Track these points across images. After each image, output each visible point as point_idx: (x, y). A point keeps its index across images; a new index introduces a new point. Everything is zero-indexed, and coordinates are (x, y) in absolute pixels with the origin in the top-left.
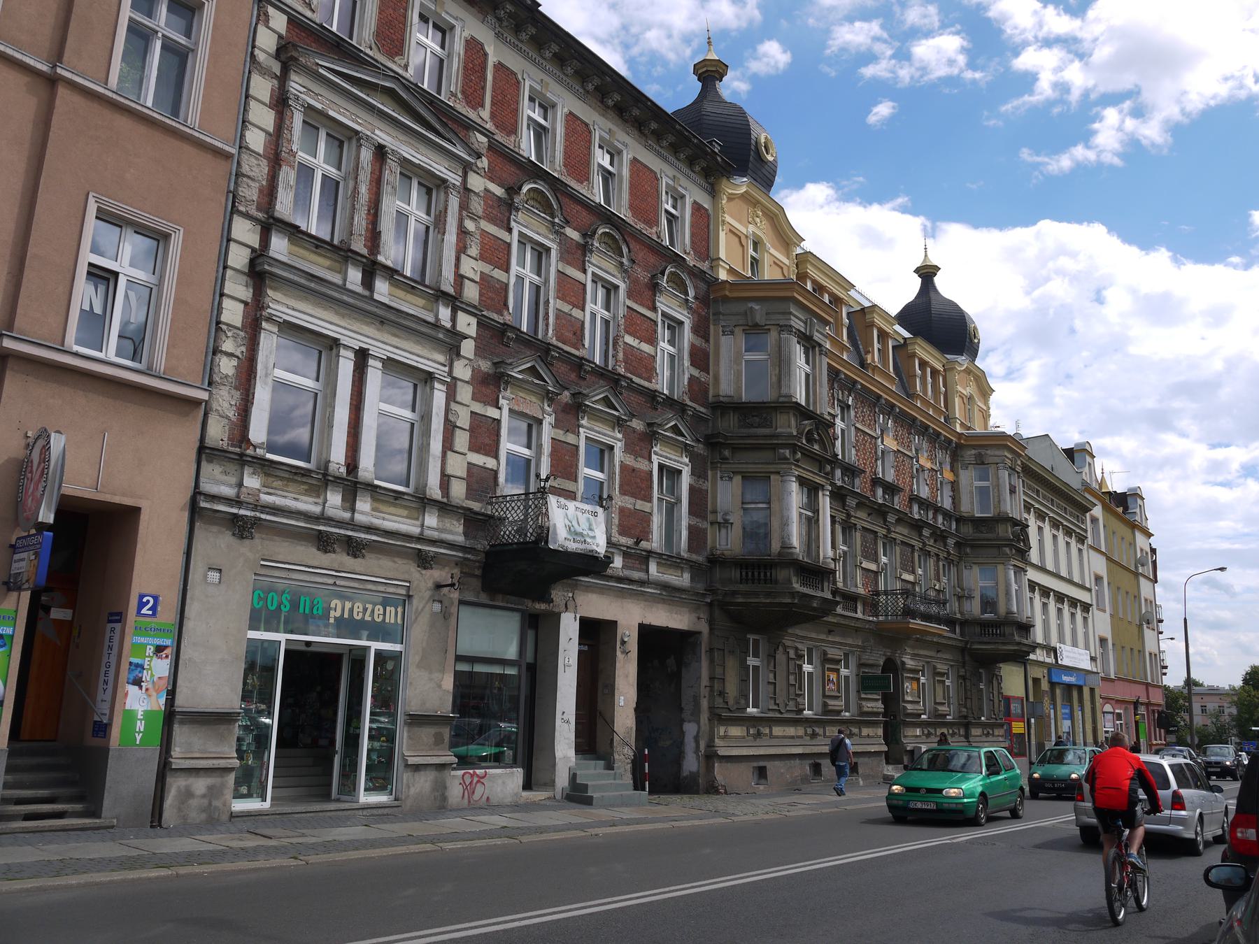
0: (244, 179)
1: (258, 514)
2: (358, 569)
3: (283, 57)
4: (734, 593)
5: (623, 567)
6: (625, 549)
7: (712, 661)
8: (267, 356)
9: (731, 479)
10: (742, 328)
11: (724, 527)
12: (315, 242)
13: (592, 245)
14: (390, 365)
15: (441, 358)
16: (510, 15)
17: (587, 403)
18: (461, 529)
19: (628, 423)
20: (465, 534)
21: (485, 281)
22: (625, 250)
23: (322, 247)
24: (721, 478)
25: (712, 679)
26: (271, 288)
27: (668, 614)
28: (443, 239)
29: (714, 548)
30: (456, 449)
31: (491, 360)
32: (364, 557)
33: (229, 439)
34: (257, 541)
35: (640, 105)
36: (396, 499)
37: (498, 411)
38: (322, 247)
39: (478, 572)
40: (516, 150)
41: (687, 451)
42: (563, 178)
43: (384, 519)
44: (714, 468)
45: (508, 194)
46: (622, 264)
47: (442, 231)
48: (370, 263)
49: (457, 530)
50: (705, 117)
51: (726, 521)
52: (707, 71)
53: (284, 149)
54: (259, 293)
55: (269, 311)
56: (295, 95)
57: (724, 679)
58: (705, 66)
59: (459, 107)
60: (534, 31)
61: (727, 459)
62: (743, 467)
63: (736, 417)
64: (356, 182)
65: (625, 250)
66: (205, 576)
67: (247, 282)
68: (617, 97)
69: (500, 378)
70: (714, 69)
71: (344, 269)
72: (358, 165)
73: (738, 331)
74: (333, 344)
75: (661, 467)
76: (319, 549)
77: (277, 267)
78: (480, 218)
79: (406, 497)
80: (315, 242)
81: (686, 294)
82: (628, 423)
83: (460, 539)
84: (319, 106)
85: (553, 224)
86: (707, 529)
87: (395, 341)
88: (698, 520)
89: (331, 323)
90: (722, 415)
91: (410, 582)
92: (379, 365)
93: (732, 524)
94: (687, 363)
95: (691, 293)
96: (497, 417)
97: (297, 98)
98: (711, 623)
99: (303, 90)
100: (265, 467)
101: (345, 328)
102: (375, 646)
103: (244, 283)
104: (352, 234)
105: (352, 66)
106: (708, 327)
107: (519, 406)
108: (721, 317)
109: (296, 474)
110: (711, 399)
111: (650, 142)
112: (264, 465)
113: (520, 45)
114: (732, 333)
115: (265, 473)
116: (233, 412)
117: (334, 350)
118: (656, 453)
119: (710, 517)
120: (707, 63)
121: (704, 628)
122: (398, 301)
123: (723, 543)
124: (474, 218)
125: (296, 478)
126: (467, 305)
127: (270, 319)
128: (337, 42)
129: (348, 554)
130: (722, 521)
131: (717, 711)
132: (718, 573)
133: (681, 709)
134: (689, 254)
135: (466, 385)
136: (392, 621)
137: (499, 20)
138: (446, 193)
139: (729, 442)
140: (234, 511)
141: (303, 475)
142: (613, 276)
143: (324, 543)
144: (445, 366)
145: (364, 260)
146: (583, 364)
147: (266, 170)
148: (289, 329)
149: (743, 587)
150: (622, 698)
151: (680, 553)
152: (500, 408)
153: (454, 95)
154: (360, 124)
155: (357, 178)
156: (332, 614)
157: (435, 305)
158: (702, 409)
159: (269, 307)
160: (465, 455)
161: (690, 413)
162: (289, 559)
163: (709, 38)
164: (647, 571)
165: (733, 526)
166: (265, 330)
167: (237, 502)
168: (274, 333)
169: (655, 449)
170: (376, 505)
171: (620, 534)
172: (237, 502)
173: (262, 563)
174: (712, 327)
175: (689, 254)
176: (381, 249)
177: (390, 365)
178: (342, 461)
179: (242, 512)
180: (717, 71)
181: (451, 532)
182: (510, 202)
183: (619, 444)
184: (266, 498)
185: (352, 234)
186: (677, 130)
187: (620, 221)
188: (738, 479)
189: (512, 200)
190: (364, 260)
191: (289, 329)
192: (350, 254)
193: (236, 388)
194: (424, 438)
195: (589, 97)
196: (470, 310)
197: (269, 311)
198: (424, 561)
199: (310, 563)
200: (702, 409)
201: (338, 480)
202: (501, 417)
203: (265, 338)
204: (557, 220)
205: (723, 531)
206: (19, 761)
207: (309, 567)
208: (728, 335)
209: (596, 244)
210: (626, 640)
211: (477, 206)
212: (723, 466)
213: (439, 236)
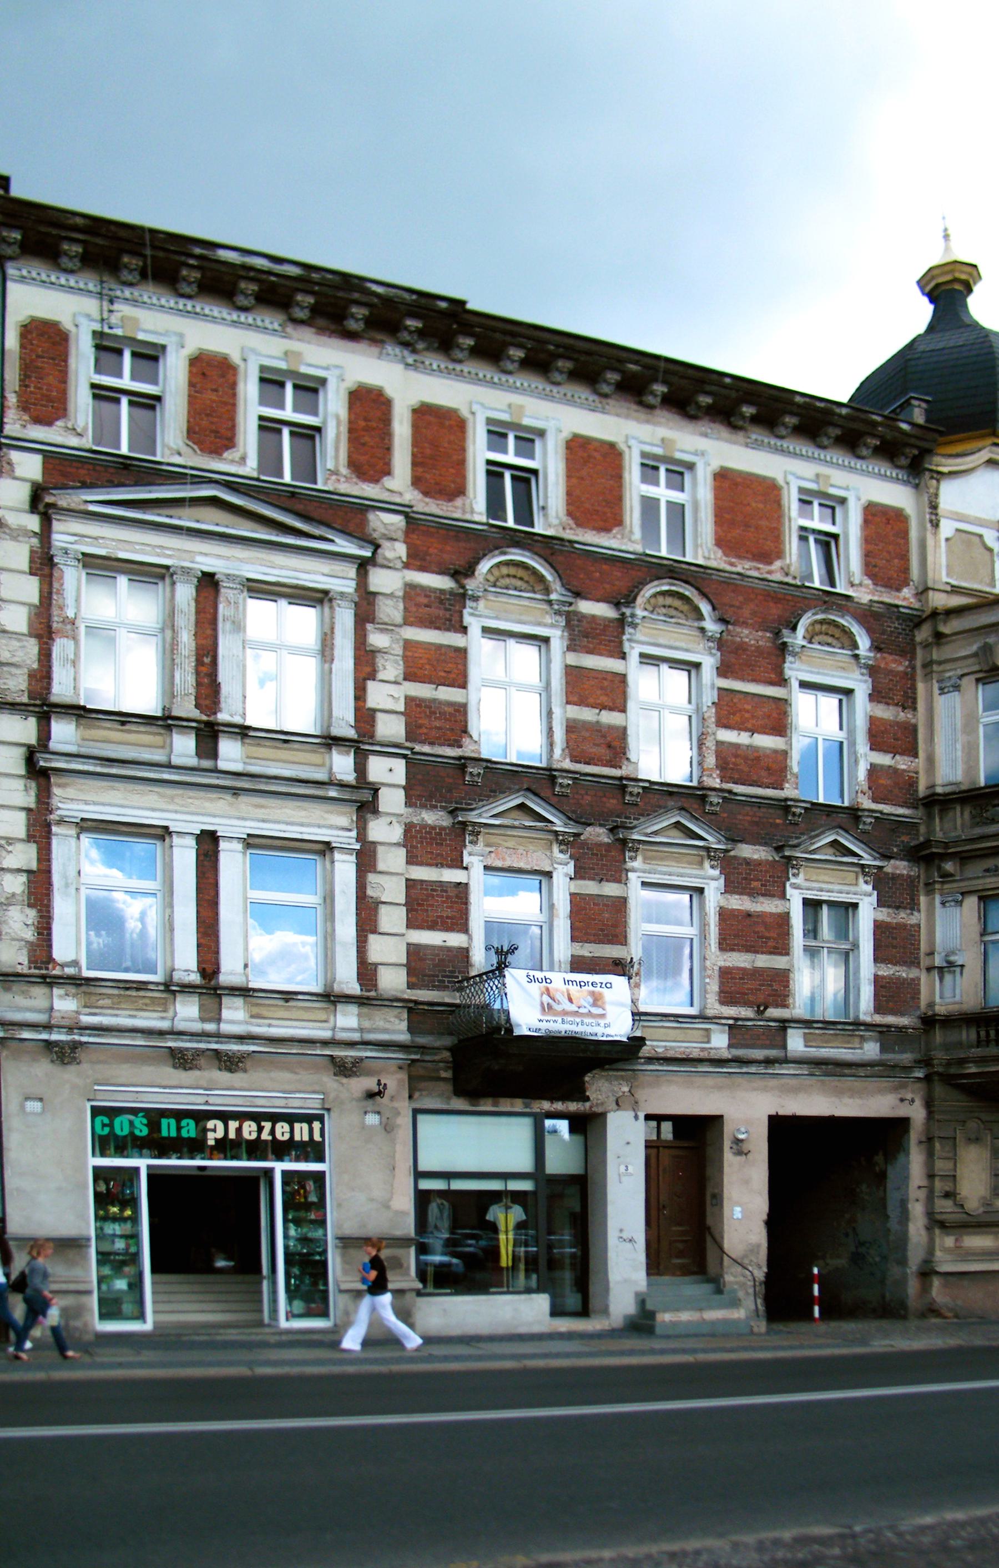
0: (5, 669)
1: (77, 1038)
2: (237, 1085)
3: (41, 508)
4: (962, 1062)
5: (730, 1046)
6: (731, 1022)
7: (930, 1154)
8: (64, 864)
9: (959, 903)
10: (973, 677)
11: (950, 972)
12: (118, 718)
13: (633, 616)
14: (251, 842)
15: (344, 821)
16: (421, 333)
17: (635, 837)
18: (404, 1025)
19: (732, 853)
20: (410, 1029)
21: (414, 708)
22: (705, 608)
23: (129, 722)
24: (943, 904)
25: (931, 1176)
26: (59, 786)
27: (833, 1099)
28: (331, 669)
29: (931, 1005)
30: (382, 930)
31: (443, 808)
32: (245, 1071)
33: (30, 962)
34: (85, 1066)
35: (708, 388)
36: (287, 1000)
37: (465, 872)
38: (129, 722)
39: (447, 1074)
40: (468, 517)
41: (865, 874)
42: (568, 535)
43: (270, 1026)
44: (930, 892)
45: (457, 581)
46: (702, 630)
47: (328, 659)
48: (202, 726)
49: (397, 1027)
50: (913, 363)
51: (951, 964)
52: (937, 286)
53: (56, 619)
54: (44, 795)
55: (59, 812)
56: (62, 549)
57: (954, 1176)
58: (933, 278)
59: (344, 488)
60: (470, 342)
61: (952, 875)
62: (979, 884)
63: (967, 815)
64: (174, 631)
65: (705, 608)
66: (22, 1107)
67: (25, 786)
68: (660, 388)
69: (464, 830)
70: (949, 278)
71: (168, 741)
72: (174, 608)
73: (968, 683)
74: (163, 834)
75: (812, 905)
76: (175, 1067)
77: (58, 761)
78: (400, 626)
79: (300, 997)
80: (118, 718)
81: (855, 646)
82: (732, 853)
83: (404, 1037)
84: (102, 552)
85: (550, 602)
86: (919, 979)
87: (261, 813)
88: (898, 968)
89: (153, 810)
90: (943, 812)
91: (324, 1094)
92: (239, 846)
93: (962, 966)
94: (862, 746)
95: (864, 642)
96: (464, 881)
97: (66, 552)
98: (929, 1104)
99: (72, 539)
100: (78, 982)
101: (176, 812)
102: (279, 1167)
103: (22, 788)
104: (173, 697)
105: (177, 487)
106: (914, 688)
107: (504, 859)
108: (935, 668)
109: (127, 989)
110: (922, 790)
111: (754, 437)
112: (80, 985)
113: (458, 367)
114: (957, 688)
115: (84, 993)
116: (30, 933)
117: (167, 840)
118: (796, 887)
119: (924, 962)
120: (935, 272)
121: (917, 1113)
122: (263, 762)
123: (948, 994)
124: (387, 628)
125: (128, 993)
126: (382, 745)
127: (61, 822)
128: (121, 463)
129: (220, 1070)
130: (945, 965)
131: (938, 1217)
132: (939, 1036)
133: (888, 1217)
134: (861, 585)
135: (393, 849)
136: (306, 1138)
137: (406, 345)
138: (331, 608)
139: (950, 851)
140: (44, 1036)
141: (138, 989)
142: (687, 650)
143: (181, 1060)
144: (350, 830)
145: (194, 724)
146: (626, 786)
147: (36, 650)
148: (87, 826)
149: (976, 1052)
150: (738, 1209)
151: (858, 1017)
152: (466, 868)
153: (335, 472)
154: (170, 557)
155: (173, 626)
156: (211, 1135)
157: (327, 756)
158: (901, 811)
159: (59, 808)
160: (403, 935)
161: (869, 820)
162: (134, 1081)
163: (946, 230)
164: (784, 1046)
165: (965, 970)
166: (57, 835)
167: (48, 1027)
168: (71, 836)
169: (793, 880)
170: (255, 1010)
171: (722, 1003)
172: (48, 1027)
173: (96, 1087)
174: (921, 687)
175: (861, 585)
176: (223, 705)
177: (251, 842)
178: (193, 965)
179: (55, 1037)
180: (956, 280)
181: (394, 1032)
182: (461, 591)
183: (714, 884)
184: (86, 1020)
185: (173, 697)
186: (799, 406)
187: (693, 568)
188: (972, 902)
189: (463, 587)
190: (194, 724)
191: (87, 826)
192: (170, 722)
193: (30, 906)
194: (329, 924)
195: (611, 402)
196: (389, 750)
197: (59, 812)
198: (343, 1069)
199: (164, 1083)
200: (901, 811)
201: (187, 988)
202: (469, 879)
203: (58, 844)
204: (553, 597)
205: (948, 978)
206: (519, 1232)
207: (165, 1087)
208: (949, 692)
209: (640, 613)
210: (741, 1137)
211: (390, 610)
212: (946, 886)
213: (327, 666)
